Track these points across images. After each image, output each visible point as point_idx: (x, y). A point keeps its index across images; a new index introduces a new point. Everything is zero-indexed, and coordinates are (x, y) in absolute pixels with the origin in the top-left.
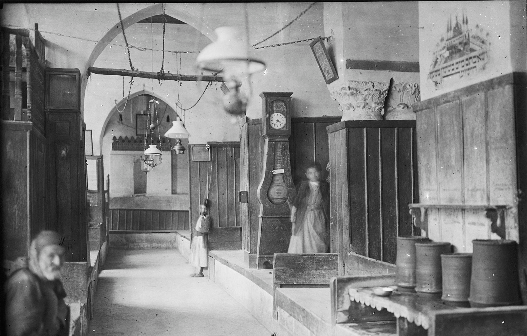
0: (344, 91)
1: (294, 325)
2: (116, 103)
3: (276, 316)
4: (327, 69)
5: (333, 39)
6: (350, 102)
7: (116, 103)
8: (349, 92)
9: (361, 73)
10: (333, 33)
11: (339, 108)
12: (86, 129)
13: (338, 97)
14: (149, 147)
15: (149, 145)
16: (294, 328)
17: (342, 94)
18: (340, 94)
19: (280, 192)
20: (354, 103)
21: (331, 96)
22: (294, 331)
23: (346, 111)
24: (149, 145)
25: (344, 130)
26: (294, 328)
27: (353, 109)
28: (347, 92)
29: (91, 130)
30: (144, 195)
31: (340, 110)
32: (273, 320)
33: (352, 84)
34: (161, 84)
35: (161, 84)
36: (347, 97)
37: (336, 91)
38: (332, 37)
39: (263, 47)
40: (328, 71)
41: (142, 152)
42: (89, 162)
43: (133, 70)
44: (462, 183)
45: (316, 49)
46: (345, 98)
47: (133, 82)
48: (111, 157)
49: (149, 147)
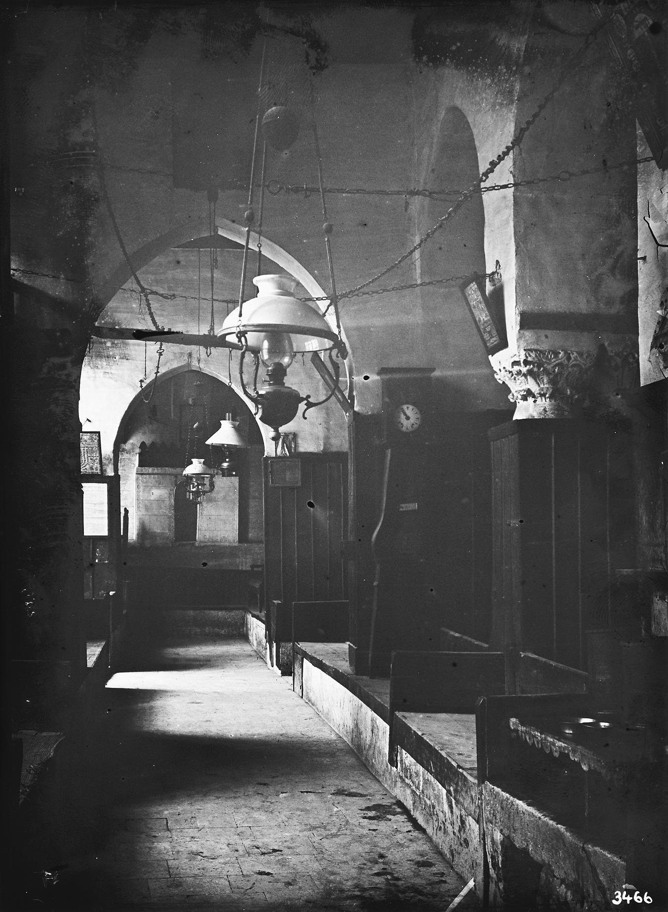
0: (516, 368)
1: (421, 778)
2: (141, 386)
3: (393, 761)
4: (488, 330)
5: (499, 277)
6: (528, 386)
7: (141, 386)
8: (524, 369)
9: (546, 337)
10: (500, 266)
11: (510, 397)
12: (83, 430)
13: (507, 379)
14: (192, 463)
15: (192, 460)
16: (421, 783)
17: (515, 372)
18: (510, 372)
19: (244, 564)
20: (535, 389)
21: (496, 376)
22: (421, 789)
23: (521, 404)
24: (192, 460)
25: (516, 435)
26: (421, 783)
27: (534, 399)
28: (521, 369)
29: (99, 433)
30: (193, 544)
31: (512, 401)
32: (389, 768)
33: (530, 356)
34: (208, 354)
35: (208, 354)
36: (523, 378)
37: (504, 368)
38: (498, 273)
39: (385, 293)
40: (489, 332)
41: (178, 470)
42: (87, 488)
43: (157, 327)
44: (383, 191)
45: (469, 295)
46: (519, 379)
47: (162, 351)
48: (137, 479)
49: (192, 463)
